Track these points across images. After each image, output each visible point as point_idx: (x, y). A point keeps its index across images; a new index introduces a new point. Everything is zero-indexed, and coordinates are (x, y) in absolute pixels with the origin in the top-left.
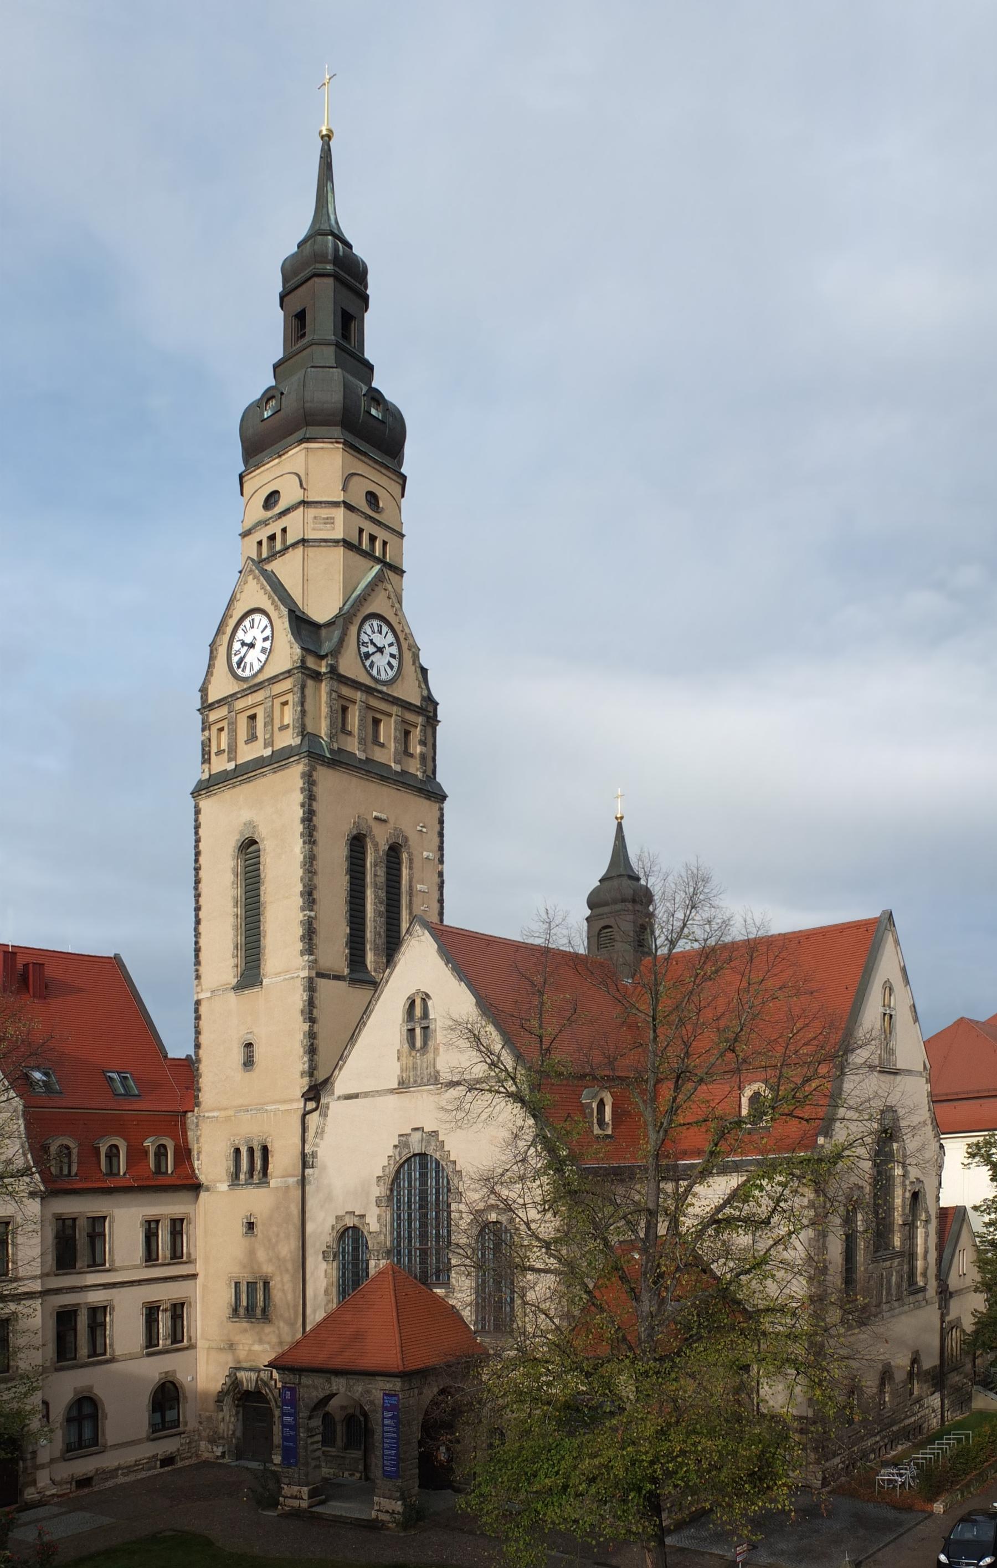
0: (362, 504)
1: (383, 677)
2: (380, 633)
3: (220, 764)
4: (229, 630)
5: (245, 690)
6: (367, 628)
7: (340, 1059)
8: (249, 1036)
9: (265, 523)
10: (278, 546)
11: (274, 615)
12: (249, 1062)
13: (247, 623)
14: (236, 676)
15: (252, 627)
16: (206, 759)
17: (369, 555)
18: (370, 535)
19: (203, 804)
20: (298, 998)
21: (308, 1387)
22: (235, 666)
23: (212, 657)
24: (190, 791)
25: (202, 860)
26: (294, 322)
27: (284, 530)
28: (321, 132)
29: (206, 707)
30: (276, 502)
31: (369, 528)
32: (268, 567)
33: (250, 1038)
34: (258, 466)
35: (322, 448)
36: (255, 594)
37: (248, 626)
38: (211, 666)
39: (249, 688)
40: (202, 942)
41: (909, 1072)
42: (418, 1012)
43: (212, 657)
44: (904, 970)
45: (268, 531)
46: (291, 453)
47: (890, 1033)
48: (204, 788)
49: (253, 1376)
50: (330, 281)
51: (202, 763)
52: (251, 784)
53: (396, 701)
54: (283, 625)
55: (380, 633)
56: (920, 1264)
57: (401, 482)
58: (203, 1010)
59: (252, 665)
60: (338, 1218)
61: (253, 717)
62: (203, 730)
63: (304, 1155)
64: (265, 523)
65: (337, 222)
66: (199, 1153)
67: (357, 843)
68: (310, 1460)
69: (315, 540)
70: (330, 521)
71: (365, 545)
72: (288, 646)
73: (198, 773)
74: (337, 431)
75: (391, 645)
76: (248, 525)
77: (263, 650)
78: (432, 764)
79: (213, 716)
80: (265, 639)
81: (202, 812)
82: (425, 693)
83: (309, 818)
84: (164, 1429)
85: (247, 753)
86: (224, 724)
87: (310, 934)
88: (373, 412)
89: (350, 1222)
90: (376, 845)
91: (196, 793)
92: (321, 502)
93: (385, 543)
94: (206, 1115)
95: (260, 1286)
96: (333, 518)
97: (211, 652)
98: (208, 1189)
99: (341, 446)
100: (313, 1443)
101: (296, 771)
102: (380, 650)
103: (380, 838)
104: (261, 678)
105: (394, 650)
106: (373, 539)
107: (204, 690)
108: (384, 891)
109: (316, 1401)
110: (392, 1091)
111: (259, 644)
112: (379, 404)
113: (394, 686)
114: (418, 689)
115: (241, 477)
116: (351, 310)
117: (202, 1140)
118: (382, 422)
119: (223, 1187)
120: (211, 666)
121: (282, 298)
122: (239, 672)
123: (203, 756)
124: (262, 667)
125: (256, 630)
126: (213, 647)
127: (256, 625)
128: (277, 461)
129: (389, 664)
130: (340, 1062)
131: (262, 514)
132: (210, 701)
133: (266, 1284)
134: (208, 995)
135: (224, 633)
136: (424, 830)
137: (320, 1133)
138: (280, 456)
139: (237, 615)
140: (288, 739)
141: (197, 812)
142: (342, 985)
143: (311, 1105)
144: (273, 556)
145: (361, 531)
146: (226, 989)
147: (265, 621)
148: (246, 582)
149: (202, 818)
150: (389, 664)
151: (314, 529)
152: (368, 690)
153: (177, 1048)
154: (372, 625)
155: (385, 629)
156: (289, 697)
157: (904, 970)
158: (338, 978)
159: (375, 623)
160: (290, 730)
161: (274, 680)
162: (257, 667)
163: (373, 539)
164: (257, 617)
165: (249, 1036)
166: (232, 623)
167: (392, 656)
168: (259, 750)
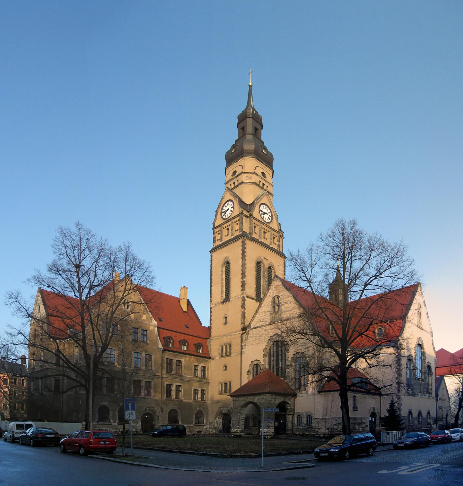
0: (260, 174)
1: (267, 221)
2: (266, 209)
3: (218, 243)
4: (221, 207)
5: (226, 221)
6: (262, 206)
7: (253, 318)
8: (226, 315)
9: (232, 179)
10: (236, 184)
11: (234, 201)
12: (226, 323)
13: (226, 204)
14: (223, 219)
15: (228, 205)
16: (214, 242)
17: (262, 188)
18: (263, 183)
19: (213, 254)
20: (240, 302)
21: (241, 401)
22: (223, 216)
23: (216, 214)
24: (210, 251)
25: (213, 269)
26: (242, 130)
27: (238, 181)
28: (249, 84)
29: (214, 228)
30: (235, 174)
31: (263, 181)
32: (233, 191)
33: (226, 316)
34: (230, 165)
35: (249, 159)
36: (229, 196)
37: (227, 205)
38: (216, 217)
39: (227, 221)
40: (212, 292)
41: (426, 331)
42: (277, 301)
43: (216, 214)
44: (424, 302)
45: (233, 181)
46: (240, 160)
47: (421, 318)
48: (213, 250)
49: (226, 409)
50: (251, 119)
51: (213, 243)
52: (227, 247)
53: (270, 228)
54: (236, 203)
55: (266, 209)
56: (430, 387)
57: (272, 172)
58: (212, 310)
59: (228, 215)
60: (252, 362)
61: (228, 229)
62: (213, 234)
63: (242, 346)
64: (232, 179)
65: (253, 106)
66: (211, 349)
67: (259, 263)
68: (240, 422)
69: (246, 182)
70: (251, 178)
71: (261, 185)
72: (238, 208)
73: (211, 246)
74: (253, 155)
75: (269, 213)
76: (227, 181)
77: (231, 211)
78: (282, 249)
79: (216, 230)
80: (232, 208)
81: (213, 256)
82: (279, 228)
83: (244, 253)
84: (198, 424)
85: (225, 239)
86: (220, 232)
87: (243, 285)
88: (264, 151)
89: (255, 362)
90: (264, 265)
91: (211, 251)
92: (248, 173)
93: (267, 187)
94: (213, 338)
95: (228, 384)
96: (252, 177)
97: (216, 213)
98: (213, 359)
99: (254, 158)
100: (242, 417)
101: (240, 242)
102: (266, 213)
103: (266, 264)
104: (230, 218)
105: (270, 214)
106: (264, 184)
107: (214, 224)
108: (267, 278)
109: (243, 404)
110: (269, 325)
111: (230, 209)
112: (266, 150)
113: (270, 224)
114: (277, 227)
115: (225, 169)
116: (257, 127)
117: (212, 346)
118: (266, 155)
119: (218, 358)
120: (216, 217)
121: (238, 124)
122: (224, 217)
123: (213, 241)
124: (231, 215)
125: (229, 206)
126: (217, 212)
127: (229, 204)
128: (236, 163)
129: (269, 218)
130: (253, 319)
131: (231, 177)
132: (216, 226)
133: (230, 383)
134: (214, 305)
135: (220, 208)
136: (279, 265)
137: (246, 339)
138: (237, 162)
139: (223, 202)
140: (238, 233)
141: (211, 256)
142: (254, 301)
143: (244, 332)
144: (235, 187)
145: (260, 182)
146: (219, 303)
147: (232, 203)
148: (226, 193)
149: (213, 258)
150: (269, 218)
151: (246, 180)
152: (263, 223)
153: (205, 323)
154: (263, 207)
155: (267, 208)
156: (238, 222)
157: (424, 302)
158: (252, 299)
159: (264, 206)
160: (239, 231)
161: (234, 218)
162: (229, 215)
163: (264, 184)
164: (229, 202)
165: (226, 315)
166: (222, 205)
167: (269, 216)
168: (230, 237)
